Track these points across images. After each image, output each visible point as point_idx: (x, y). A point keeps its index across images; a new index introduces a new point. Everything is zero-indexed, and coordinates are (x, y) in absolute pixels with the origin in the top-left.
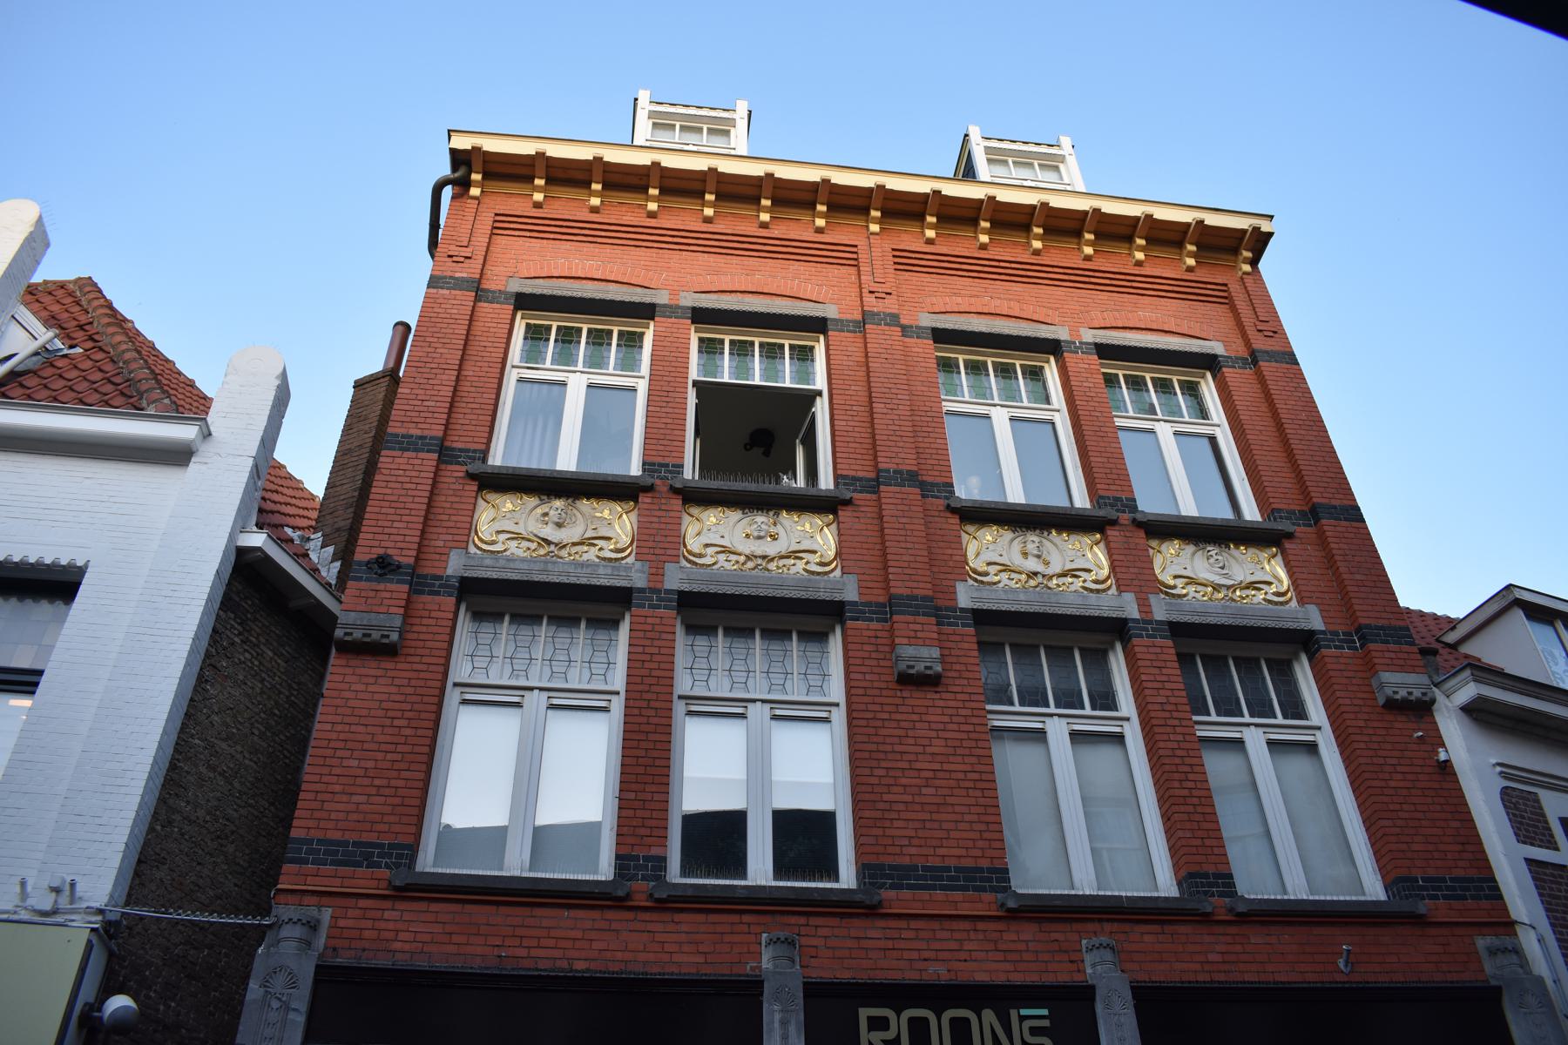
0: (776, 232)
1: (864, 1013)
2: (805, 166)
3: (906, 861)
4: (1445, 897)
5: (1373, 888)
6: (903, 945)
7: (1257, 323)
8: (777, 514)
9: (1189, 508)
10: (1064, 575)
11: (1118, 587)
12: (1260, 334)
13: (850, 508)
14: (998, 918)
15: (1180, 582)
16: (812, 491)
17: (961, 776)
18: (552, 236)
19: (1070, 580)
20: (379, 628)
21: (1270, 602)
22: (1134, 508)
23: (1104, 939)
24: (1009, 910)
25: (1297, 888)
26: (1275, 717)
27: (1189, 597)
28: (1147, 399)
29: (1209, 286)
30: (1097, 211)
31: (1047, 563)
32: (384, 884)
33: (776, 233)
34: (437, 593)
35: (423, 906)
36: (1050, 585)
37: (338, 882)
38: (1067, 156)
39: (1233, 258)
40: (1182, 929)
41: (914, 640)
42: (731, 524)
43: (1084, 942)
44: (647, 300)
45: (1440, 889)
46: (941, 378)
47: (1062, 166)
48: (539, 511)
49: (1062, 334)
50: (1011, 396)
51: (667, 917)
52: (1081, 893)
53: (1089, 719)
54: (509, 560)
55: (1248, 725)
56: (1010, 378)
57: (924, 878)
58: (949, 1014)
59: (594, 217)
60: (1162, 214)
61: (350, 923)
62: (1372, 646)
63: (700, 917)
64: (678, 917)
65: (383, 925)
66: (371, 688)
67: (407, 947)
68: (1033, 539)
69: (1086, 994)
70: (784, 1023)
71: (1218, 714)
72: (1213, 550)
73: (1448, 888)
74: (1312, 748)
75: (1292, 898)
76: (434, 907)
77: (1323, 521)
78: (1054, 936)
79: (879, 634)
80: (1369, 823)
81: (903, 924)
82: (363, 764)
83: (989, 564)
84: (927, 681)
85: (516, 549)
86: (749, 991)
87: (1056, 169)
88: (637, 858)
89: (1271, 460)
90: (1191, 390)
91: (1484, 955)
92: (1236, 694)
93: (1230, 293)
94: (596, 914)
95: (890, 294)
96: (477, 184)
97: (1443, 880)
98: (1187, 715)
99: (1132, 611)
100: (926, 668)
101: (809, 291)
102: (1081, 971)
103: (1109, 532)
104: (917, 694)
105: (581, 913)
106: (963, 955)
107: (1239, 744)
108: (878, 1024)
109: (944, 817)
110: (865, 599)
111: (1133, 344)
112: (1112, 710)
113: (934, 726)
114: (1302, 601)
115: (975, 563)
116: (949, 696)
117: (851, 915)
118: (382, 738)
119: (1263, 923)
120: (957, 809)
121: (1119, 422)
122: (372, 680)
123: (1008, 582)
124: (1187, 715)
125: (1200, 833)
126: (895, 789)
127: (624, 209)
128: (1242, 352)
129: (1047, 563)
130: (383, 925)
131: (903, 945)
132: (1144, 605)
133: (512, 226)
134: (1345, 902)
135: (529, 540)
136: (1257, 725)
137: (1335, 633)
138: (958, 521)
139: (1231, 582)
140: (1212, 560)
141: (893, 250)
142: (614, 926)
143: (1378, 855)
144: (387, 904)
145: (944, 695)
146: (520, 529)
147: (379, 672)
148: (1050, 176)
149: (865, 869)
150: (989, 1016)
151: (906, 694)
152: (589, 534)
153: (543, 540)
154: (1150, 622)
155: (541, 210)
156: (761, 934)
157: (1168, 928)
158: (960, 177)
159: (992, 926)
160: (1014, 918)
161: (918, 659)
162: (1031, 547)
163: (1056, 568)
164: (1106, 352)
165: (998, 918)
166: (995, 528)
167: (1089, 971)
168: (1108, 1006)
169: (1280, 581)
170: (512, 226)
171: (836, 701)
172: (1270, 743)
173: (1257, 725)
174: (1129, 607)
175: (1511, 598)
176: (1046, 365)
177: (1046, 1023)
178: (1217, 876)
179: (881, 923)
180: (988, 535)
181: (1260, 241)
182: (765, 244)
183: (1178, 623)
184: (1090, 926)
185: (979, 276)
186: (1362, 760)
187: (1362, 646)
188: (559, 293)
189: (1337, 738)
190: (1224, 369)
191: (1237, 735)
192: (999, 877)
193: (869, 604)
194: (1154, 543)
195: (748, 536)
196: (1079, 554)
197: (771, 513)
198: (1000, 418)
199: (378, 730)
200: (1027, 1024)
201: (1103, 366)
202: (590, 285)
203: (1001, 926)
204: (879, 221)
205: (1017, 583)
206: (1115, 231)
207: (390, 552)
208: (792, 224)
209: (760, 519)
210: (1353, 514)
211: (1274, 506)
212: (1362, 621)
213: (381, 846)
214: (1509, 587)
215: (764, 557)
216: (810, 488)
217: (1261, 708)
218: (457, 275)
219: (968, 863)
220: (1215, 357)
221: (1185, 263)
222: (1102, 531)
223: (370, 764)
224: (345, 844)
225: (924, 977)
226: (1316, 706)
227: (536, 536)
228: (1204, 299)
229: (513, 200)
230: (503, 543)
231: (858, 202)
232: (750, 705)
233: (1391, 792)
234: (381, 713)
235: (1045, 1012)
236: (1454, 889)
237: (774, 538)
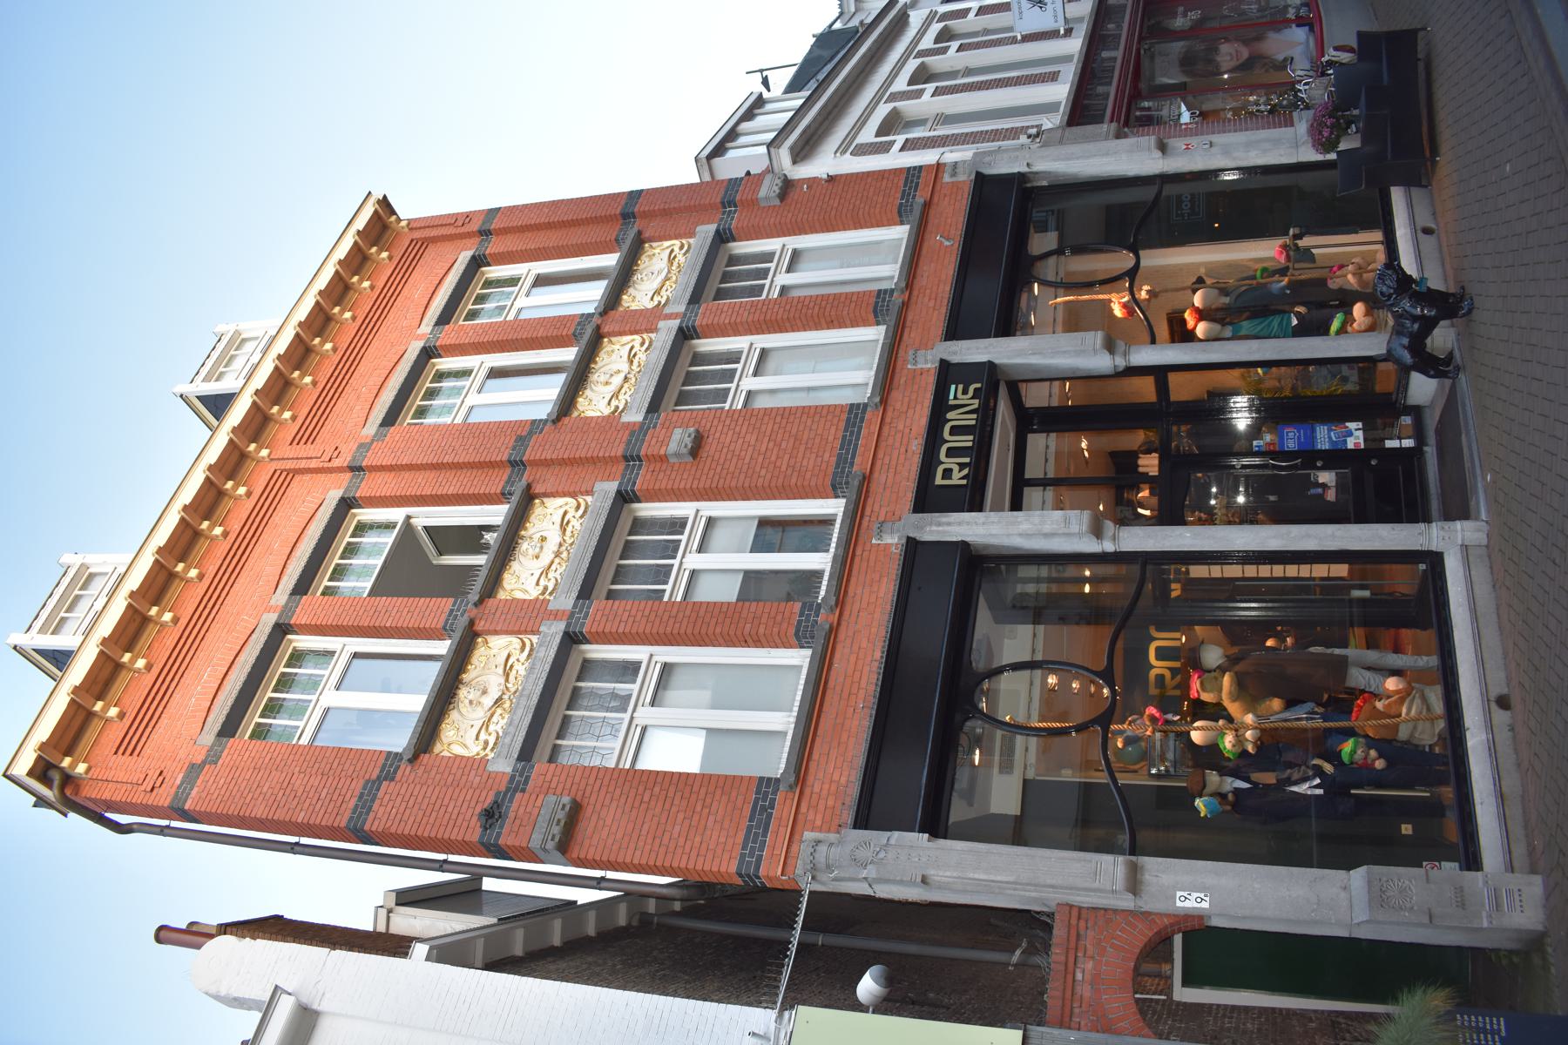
0: (236, 527)
1: (939, 481)
2: (205, 451)
3: (834, 459)
4: (916, 191)
5: (899, 233)
6: (894, 463)
7: (143, 788)
8: (522, 538)
9: (416, 702)
10: (507, 676)
11: (533, 632)
12: (155, 791)
13: (534, 486)
14: (884, 410)
15: (614, 403)
16: (502, 531)
17: (776, 426)
18: (160, 709)
19: (514, 672)
20: (554, 812)
21: (581, 517)
22: (397, 756)
23: (911, 353)
24: (881, 402)
25: (784, 721)
26: (680, 541)
27: (559, 578)
28: (279, 729)
29: (328, 388)
30: (160, 551)
31: (619, 371)
32: (790, 795)
33: (237, 527)
34: (528, 778)
35: (812, 765)
36: (513, 690)
37: (782, 829)
38: (86, 561)
39: (390, 231)
40: (910, 318)
41: (665, 442)
42: (461, 719)
43: (909, 366)
44: (268, 630)
45: (850, 441)
46: (271, 740)
47: (92, 570)
48: (463, 710)
49: (270, 619)
50: (313, 684)
51: (849, 600)
52: (793, 726)
53: (689, 538)
54: (506, 733)
55: (681, 563)
56: (281, 706)
57: (848, 450)
58: (942, 456)
59: (155, 671)
60: (187, 496)
61: (819, 817)
62: (738, 198)
63: (853, 580)
64: (851, 593)
65: (825, 792)
66: (608, 822)
67: (846, 773)
68: (464, 693)
69: (945, 365)
70: (939, 524)
71: (682, 533)
72: (636, 277)
73: (910, 188)
74: (711, 522)
75: (842, 509)
76: (815, 756)
77: (636, 209)
78: (902, 381)
79: (651, 469)
80: (858, 225)
81: (879, 463)
82: (679, 820)
83: (537, 584)
84: (697, 447)
85: (499, 724)
86: (913, 547)
87: (92, 576)
88: (799, 622)
89: (576, 236)
90: (297, 658)
91: (954, 179)
92: (661, 541)
93: (285, 470)
94: (839, 647)
95: (161, 772)
96: (74, 765)
97: (904, 191)
98: (662, 606)
99: (675, 323)
100: (689, 436)
101: (298, 521)
102: (929, 370)
103: (537, 491)
104: (707, 448)
105: (838, 655)
106: (907, 430)
107: (694, 574)
108: (947, 473)
109: (805, 437)
110: (619, 475)
111: (443, 303)
112: (671, 570)
113: (734, 439)
114: (692, 234)
115: (533, 593)
116: (713, 429)
117: (867, 491)
118: (658, 810)
119: (914, 277)
120: (801, 428)
121: (305, 741)
122: (601, 822)
123: (500, 725)
124: (662, 606)
125: (847, 303)
126: (778, 464)
127: (156, 645)
128: (477, 240)
129: (619, 371)
130: (825, 792)
131: (894, 463)
132: (556, 615)
133: (133, 742)
134: (789, 753)
135: (492, 715)
136: (683, 557)
137: (722, 219)
138: (427, 755)
139: (666, 270)
140: (645, 278)
141: (116, 753)
142: (851, 634)
143: (879, 224)
144: (807, 791)
145: (592, 801)
146: (478, 724)
147: (594, 818)
148: (97, 584)
149: (834, 491)
150: (950, 415)
151: (705, 455)
152: (500, 670)
153: (495, 703)
154: (572, 614)
155: (128, 715)
156: (872, 545)
157: (908, 323)
158: (60, 674)
159: (889, 414)
160: (804, 779)
161: (681, 441)
162: (603, 378)
163: (625, 367)
164: (303, 586)
165: (884, 410)
166: (443, 725)
167: (929, 366)
168: (955, 353)
169: (633, 340)
170: (133, 742)
171: (694, 511)
172: (700, 550)
173: (683, 557)
174: (554, 631)
175: (705, 161)
176: (294, 644)
177: (961, 387)
178: (850, 411)
179: (876, 475)
180: (448, 732)
181: (384, 203)
182: (244, 538)
183: (691, 296)
184: (899, 363)
185: (339, 393)
186: (816, 218)
187: (736, 206)
188: (230, 703)
189: (795, 235)
190: (487, 252)
191: (744, 393)
192: (766, 785)
193: (623, 476)
194: (438, 748)
195: (537, 557)
196: (492, 659)
197: (520, 541)
198: (330, 698)
199: (650, 813)
200: (959, 395)
201: (314, 594)
202: (232, 676)
203: (890, 409)
204: (380, 251)
205: (503, 718)
206: (185, 542)
207: (478, 810)
208: (230, 515)
209: (524, 546)
210: (635, 196)
211: (613, 239)
212: (718, 200)
213: (757, 800)
214: (697, 160)
215: (560, 545)
216: (490, 551)
217: (671, 550)
218: (178, 782)
219: (842, 425)
220: (473, 257)
221: (217, 536)
222: (477, 635)
223: (681, 816)
224: (749, 828)
225: (919, 451)
226: (680, 508)
227: (490, 709)
228: (418, 257)
229: (103, 740)
230: (490, 734)
231: (162, 577)
232: (684, 567)
233: (841, 207)
234: (634, 812)
235: (953, 387)
236: (912, 181)
237: (543, 539)
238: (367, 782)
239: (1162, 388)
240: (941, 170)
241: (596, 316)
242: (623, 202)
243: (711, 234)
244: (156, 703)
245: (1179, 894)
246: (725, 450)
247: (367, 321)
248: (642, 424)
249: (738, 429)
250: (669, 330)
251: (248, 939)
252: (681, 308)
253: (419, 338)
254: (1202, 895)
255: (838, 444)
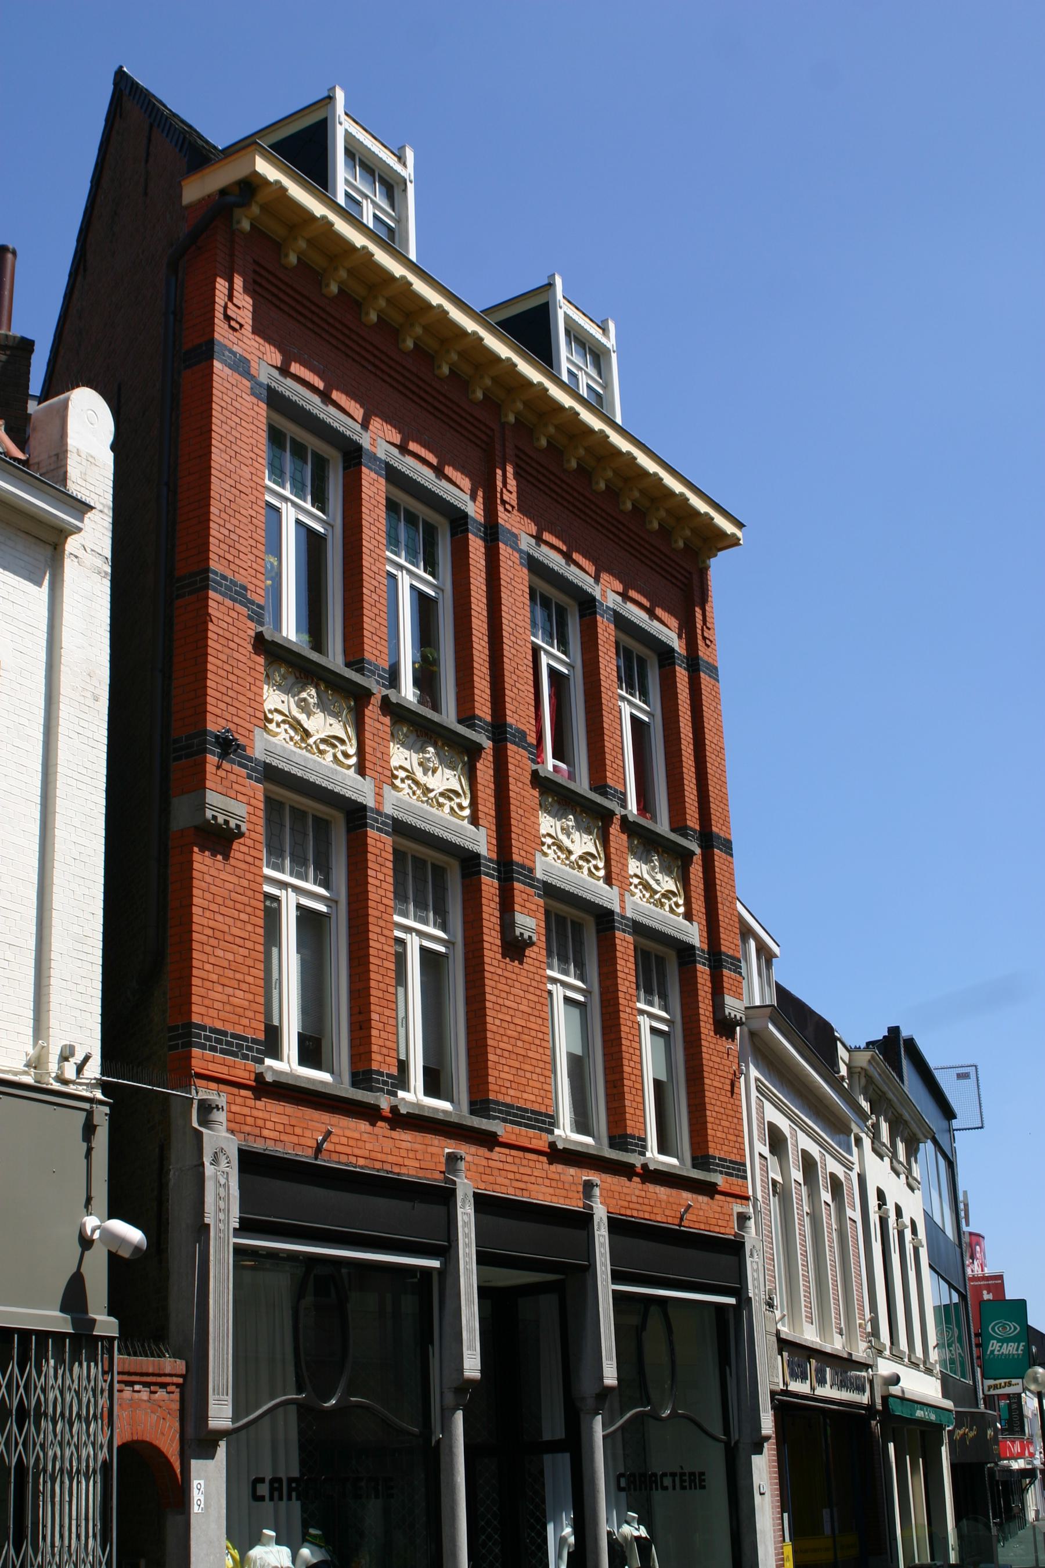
154: (379, 812)
178: (551, 1117)
219: (536, 1107)
236: (734, 1169)
238: (245, 589)
239: (554, 1447)
240: (743, 1201)
241: (623, 812)
242: (722, 834)
243: (475, 848)
244: (293, 303)
245: (202, 1482)
246: (514, 977)
247: (620, 526)
248: (533, 879)
249: (531, 989)
250: (476, 841)
251: (112, 454)
252: (388, 809)
253: (604, 594)
254: (202, 1506)
255: (521, 1104)
